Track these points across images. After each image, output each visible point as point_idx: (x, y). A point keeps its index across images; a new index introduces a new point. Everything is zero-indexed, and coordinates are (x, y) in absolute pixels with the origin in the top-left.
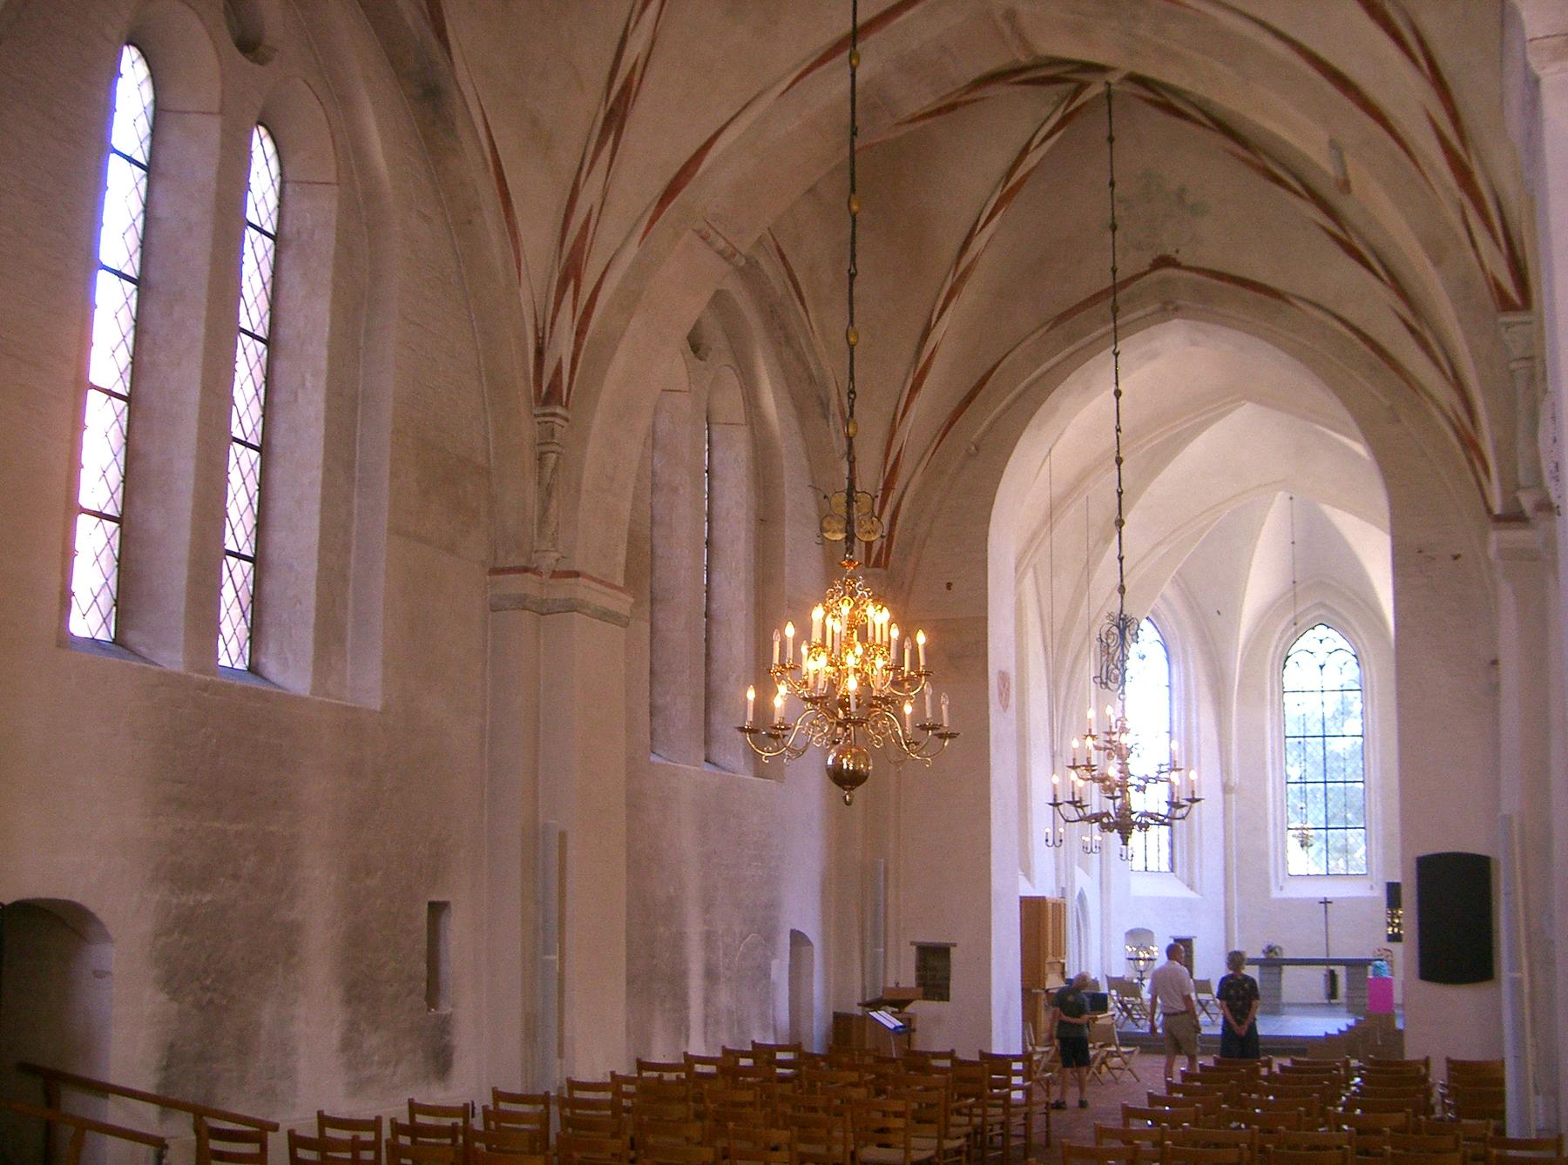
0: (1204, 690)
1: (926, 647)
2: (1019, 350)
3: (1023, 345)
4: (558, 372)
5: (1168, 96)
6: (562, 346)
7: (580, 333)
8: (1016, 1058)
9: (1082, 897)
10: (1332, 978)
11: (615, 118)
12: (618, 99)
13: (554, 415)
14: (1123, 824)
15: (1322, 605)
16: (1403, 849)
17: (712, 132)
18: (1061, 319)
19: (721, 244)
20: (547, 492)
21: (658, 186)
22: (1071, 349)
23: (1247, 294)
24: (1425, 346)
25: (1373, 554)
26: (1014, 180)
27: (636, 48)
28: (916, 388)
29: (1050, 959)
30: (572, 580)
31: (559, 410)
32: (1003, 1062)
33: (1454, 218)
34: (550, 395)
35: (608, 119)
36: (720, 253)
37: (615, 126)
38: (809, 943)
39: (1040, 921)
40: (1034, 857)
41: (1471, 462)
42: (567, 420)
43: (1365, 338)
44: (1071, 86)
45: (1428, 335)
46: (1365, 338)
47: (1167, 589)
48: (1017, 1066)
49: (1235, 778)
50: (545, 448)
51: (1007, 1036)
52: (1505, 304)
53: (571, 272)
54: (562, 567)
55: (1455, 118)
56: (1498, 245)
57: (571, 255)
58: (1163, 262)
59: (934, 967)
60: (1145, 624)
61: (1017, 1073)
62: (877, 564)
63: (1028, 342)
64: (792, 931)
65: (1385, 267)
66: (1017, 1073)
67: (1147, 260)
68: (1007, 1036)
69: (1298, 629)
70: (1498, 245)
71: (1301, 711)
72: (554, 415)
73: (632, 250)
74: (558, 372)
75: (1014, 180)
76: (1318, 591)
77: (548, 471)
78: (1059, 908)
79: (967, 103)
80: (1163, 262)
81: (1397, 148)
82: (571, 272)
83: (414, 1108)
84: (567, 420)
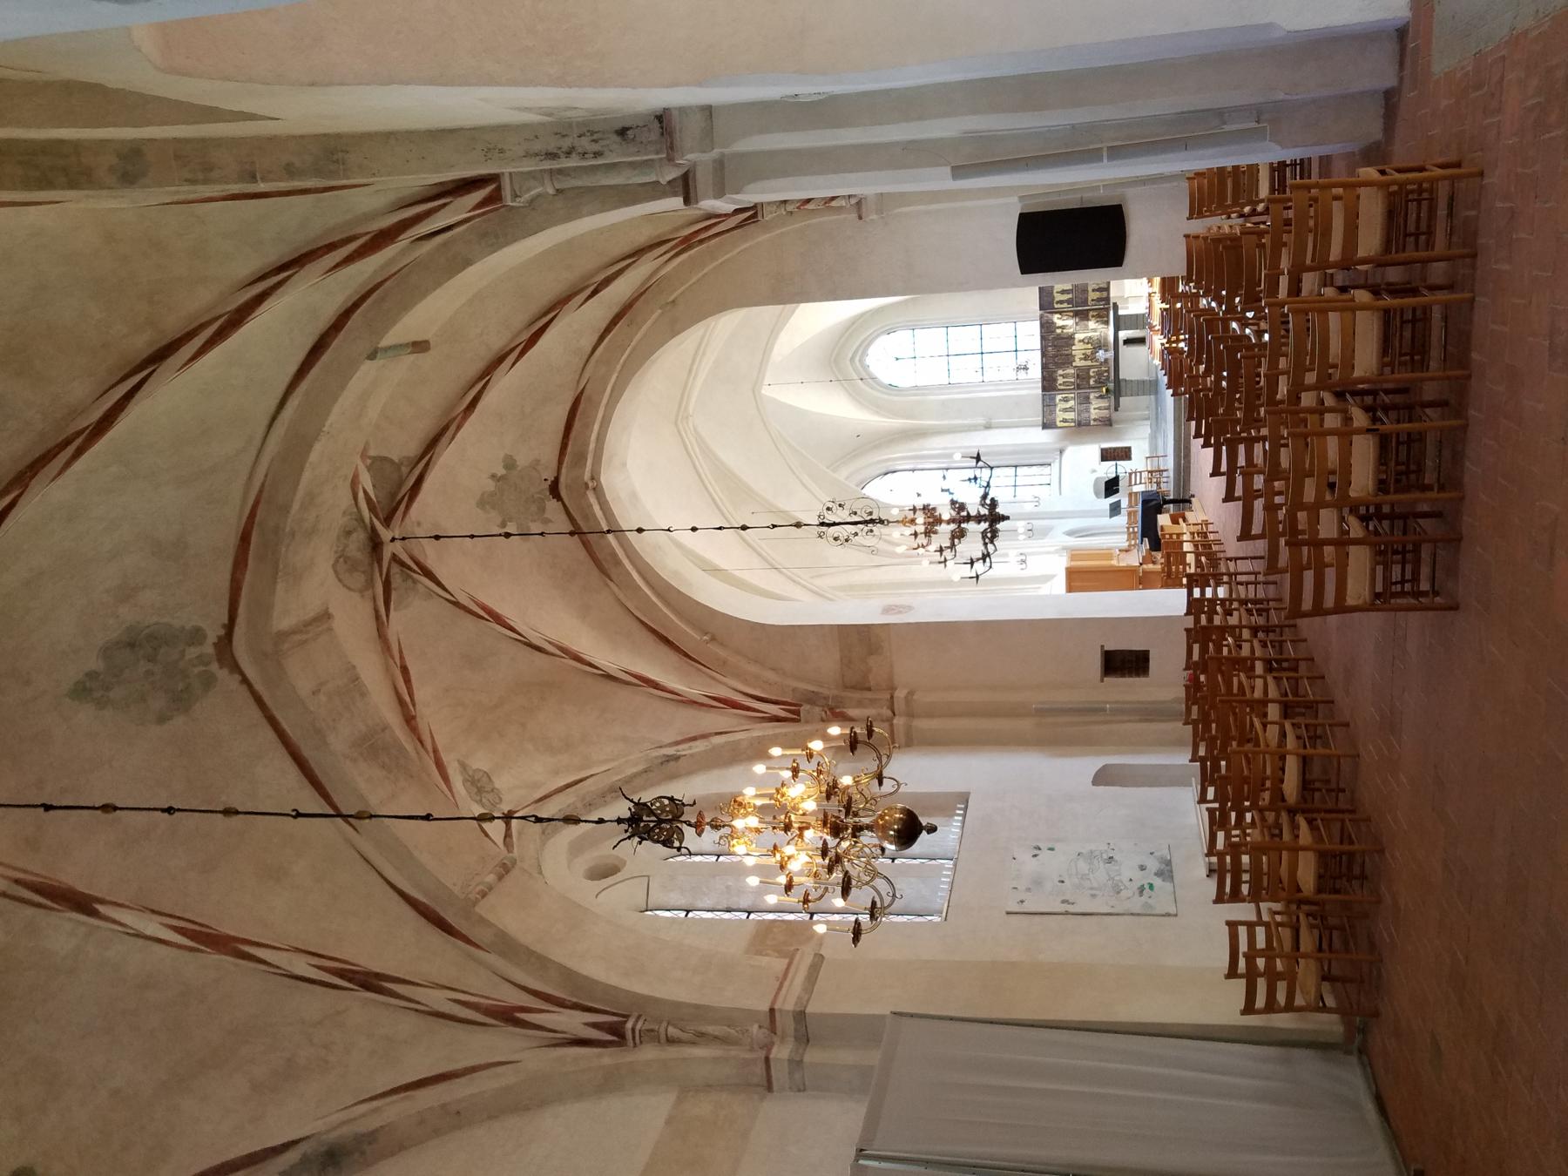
0: (915, 445)
1: (784, 747)
2: (629, 605)
3: (624, 600)
4: (595, 1025)
5: (403, 491)
6: (573, 1022)
7: (561, 1003)
8: (1190, 594)
9: (1070, 533)
10: (1128, 342)
11: (370, 982)
12: (350, 981)
13: (633, 1030)
14: (993, 517)
15: (852, 359)
16: (1015, 285)
17: (388, 888)
18: (603, 571)
19: (491, 878)
20: (701, 1038)
21: (436, 937)
22: (626, 562)
23: (577, 425)
24: (607, 281)
25: (816, 319)
26: (482, 613)
27: (302, 966)
28: (655, 685)
29: (1114, 562)
30: (777, 1015)
31: (629, 1025)
32: (1194, 606)
33: (428, 246)
34: (616, 1034)
35: (367, 987)
36: (500, 878)
37: (375, 982)
38: (1105, 767)
39: (1079, 579)
40: (1029, 580)
41: (701, 242)
42: (639, 1017)
43: (607, 330)
44: (395, 569)
45: (601, 277)
46: (607, 330)
47: (841, 475)
48: (1197, 593)
49: (981, 421)
50: (663, 1036)
51: (1173, 602)
52: (495, 198)
53: (508, 1016)
54: (767, 1023)
55: (332, 247)
56: (445, 205)
57: (495, 1018)
58: (554, 490)
59: (1124, 663)
60: (868, 491)
61: (1203, 593)
62: (797, 713)
63: (621, 597)
64: (1070, 589)
65: (545, 314)
66: (1203, 593)
67: (552, 504)
68: (1173, 602)
69: (868, 378)
70: (445, 205)
71: (930, 373)
72: (633, 1030)
73: (491, 958)
74: (595, 1025)
75: (482, 613)
76: (841, 360)
77: (684, 1036)
78: (1074, 554)
79: (402, 657)
80: (554, 490)
81: (369, 301)
82: (508, 1016)
83: (1216, 472)
84: (639, 1017)
